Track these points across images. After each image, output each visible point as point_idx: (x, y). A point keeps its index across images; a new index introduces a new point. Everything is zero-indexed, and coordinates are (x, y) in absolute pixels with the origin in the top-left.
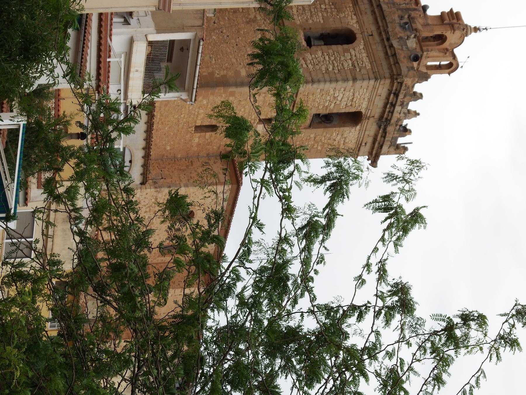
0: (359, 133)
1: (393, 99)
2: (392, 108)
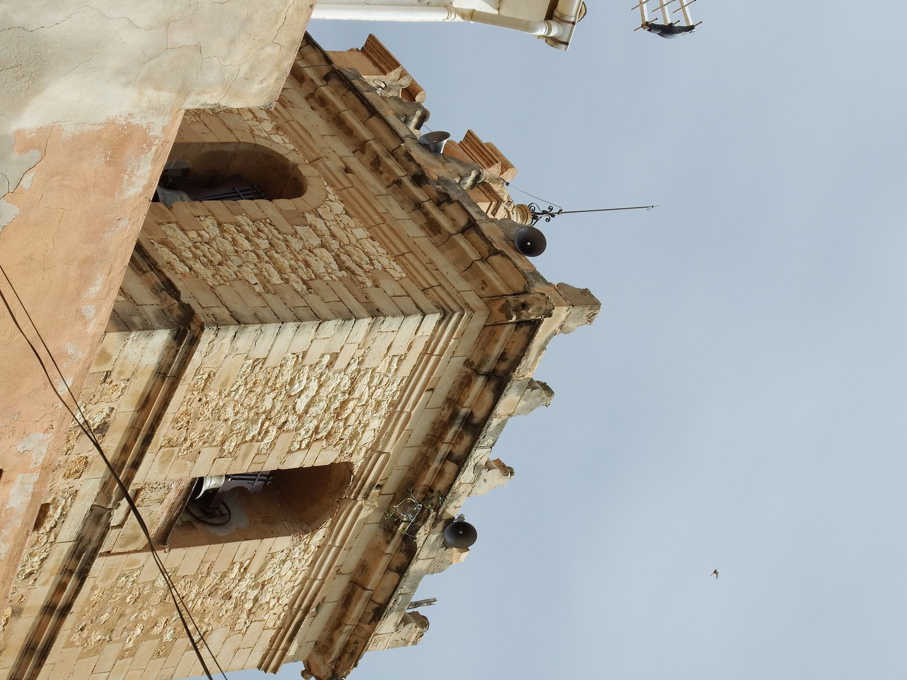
0: (314, 562)
1: (480, 397)
2: (467, 440)
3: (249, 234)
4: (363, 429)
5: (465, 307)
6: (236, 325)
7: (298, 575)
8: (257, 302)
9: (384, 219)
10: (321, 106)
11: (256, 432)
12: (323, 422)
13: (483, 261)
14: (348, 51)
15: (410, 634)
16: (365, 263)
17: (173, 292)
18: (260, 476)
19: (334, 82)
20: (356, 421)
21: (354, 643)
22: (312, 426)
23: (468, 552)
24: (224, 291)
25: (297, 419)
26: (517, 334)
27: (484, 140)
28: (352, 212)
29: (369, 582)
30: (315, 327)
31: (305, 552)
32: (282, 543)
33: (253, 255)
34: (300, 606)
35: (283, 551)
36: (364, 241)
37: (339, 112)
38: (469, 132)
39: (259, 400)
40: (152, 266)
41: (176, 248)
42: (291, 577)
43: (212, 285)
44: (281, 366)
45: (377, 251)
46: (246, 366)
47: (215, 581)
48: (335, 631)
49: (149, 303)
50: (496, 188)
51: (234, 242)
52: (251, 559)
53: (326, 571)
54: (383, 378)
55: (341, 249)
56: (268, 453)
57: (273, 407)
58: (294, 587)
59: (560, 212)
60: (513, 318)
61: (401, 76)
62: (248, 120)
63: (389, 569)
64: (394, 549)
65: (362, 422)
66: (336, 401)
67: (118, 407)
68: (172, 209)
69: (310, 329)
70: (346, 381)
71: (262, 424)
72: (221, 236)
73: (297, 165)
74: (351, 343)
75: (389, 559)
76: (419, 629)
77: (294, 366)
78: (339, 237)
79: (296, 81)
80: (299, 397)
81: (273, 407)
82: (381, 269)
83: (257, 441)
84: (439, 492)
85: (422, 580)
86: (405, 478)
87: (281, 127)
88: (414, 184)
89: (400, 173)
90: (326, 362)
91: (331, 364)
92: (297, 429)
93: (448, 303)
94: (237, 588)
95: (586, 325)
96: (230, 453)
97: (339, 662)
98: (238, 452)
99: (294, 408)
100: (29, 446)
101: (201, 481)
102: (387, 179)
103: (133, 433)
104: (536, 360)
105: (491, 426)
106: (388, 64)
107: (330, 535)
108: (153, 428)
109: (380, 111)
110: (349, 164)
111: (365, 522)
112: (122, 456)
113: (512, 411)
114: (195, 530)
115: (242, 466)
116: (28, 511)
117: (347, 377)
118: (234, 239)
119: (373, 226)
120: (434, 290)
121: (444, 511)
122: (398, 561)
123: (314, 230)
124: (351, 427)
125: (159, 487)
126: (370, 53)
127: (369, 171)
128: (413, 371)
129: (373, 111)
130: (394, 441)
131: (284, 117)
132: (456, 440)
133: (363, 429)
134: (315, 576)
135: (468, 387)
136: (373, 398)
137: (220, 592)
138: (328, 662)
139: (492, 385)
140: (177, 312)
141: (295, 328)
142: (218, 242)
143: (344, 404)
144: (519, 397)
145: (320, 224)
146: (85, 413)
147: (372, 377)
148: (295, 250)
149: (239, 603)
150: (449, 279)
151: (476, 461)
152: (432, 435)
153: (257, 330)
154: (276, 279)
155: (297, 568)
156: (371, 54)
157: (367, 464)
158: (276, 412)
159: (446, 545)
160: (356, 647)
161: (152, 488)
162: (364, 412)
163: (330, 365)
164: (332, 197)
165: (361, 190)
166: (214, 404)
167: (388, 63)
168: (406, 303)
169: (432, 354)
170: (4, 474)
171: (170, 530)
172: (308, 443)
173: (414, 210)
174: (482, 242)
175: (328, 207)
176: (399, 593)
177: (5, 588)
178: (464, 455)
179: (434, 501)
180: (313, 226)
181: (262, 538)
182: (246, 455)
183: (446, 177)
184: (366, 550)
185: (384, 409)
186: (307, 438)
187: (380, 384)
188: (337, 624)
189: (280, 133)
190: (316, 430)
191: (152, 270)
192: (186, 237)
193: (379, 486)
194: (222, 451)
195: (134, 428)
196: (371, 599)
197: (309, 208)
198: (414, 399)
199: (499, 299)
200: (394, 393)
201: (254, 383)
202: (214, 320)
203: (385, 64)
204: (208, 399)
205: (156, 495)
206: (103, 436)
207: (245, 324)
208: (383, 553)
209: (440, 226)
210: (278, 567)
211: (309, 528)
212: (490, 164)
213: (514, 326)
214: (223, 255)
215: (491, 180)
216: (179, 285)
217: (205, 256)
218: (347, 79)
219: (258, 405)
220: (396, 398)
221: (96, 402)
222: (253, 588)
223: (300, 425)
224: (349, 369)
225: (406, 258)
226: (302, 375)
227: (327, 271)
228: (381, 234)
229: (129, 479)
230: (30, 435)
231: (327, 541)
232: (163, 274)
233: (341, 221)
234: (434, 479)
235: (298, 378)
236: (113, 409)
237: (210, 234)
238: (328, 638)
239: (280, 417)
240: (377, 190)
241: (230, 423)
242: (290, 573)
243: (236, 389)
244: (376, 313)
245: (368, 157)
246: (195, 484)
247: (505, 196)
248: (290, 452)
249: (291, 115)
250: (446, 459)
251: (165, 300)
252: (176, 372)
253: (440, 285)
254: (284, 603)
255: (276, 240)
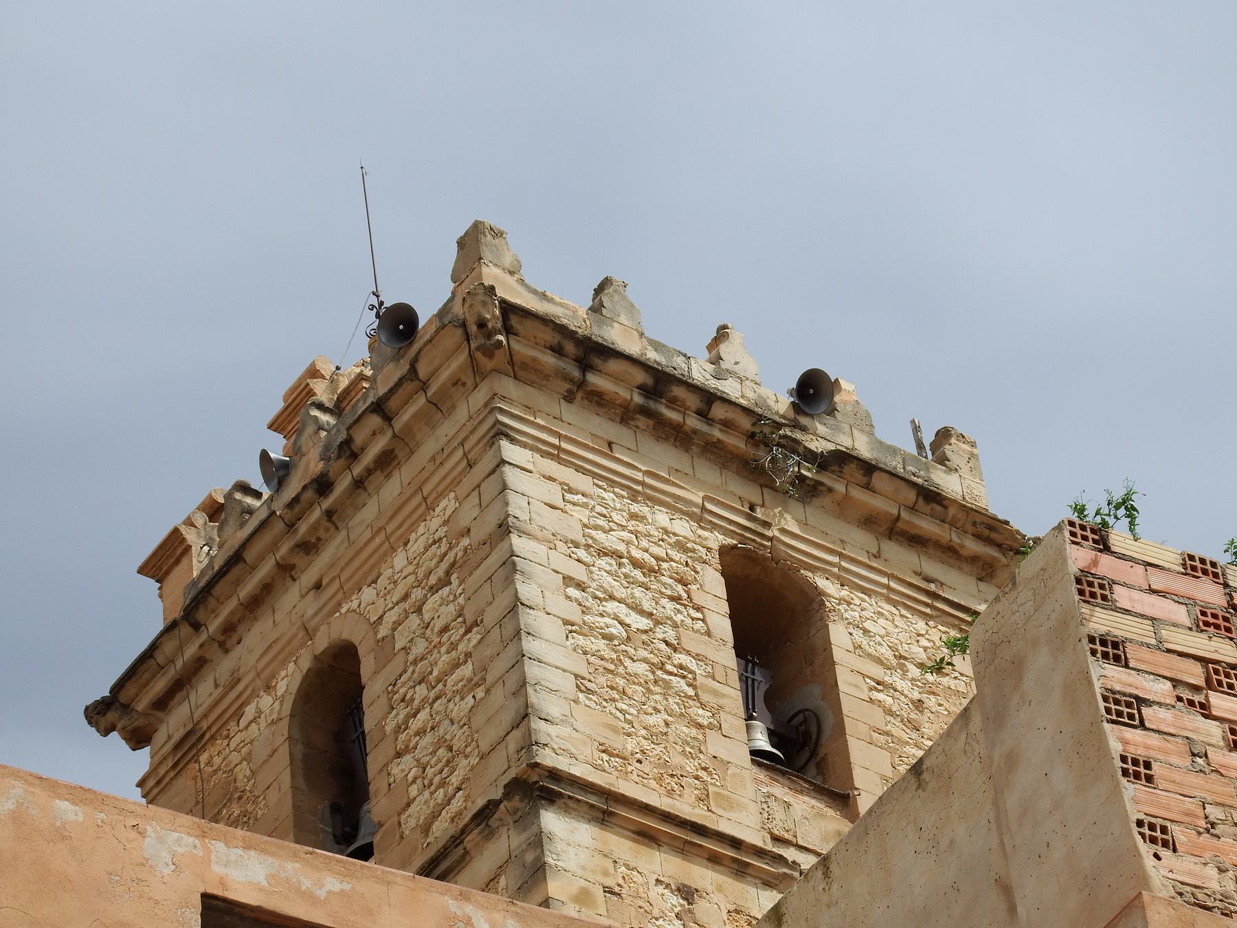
1: (616, 379)
2: (678, 391)
3: (408, 713)
4: (671, 535)
5: (489, 408)
6: (529, 721)
7: (883, 611)
8: (498, 693)
9: (381, 529)
10: (235, 631)
11: (682, 682)
12: (664, 590)
13: (427, 388)
14: (162, 601)
15: (960, 452)
16: (439, 550)
17: (490, 810)
18: (747, 672)
19: (201, 615)
20: (660, 546)
21: (975, 526)
22: (670, 605)
23: (840, 380)
24: (487, 739)
25: (660, 626)
26: (522, 333)
27: (280, 405)
28: (374, 573)
29: (888, 513)
30: (528, 610)
31: (851, 603)
32: (839, 635)
33: (436, 705)
34: (927, 605)
35: (851, 634)
36: (410, 554)
37: (242, 604)
38: (270, 427)
39: (636, 680)
40: (456, 843)
41: (432, 812)
42: (887, 619)
43: (478, 758)
44: (585, 653)
45: (422, 535)
46: (587, 702)
47: (897, 724)
48: (961, 555)
49: (506, 842)
50: (344, 383)
51: (420, 733)
52: (864, 676)
53: (876, 573)
54: (596, 513)
55: (422, 585)
56: (711, 663)
57: (645, 660)
58: (900, 615)
59: (376, 295)
60: (500, 339)
61: (192, 525)
62: (259, 730)
63: (867, 487)
64: (838, 481)
65: (660, 537)
66: (633, 574)
67: (655, 873)
68: (382, 822)
69: (531, 617)
70: (603, 563)
71: (671, 674)
72: (414, 752)
73: (315, 656)
74: (548, 559)
75: (853, 487)
76: (953, 441)
77: (585, 635)
78: (406, 589)
79: (205, 668)
80: (629, 626)
81: (645, 660)
82: (446, 527)
83: (695, 679)
84: (754, 425)
85: (884, 441)
86: (738, 473)
87: (267, 683)
88: (330, 492)
89: (316, 514)
90: (577, 592)
91: (580, 585)
92: (675, 626)
93: (485, 431)
94: (906, 692)
95: (507, 239)
96: (713, 715)
97: (1004, 546)
98: (711, 704)
99: (646, 632)
100: (165, 856)
101: (756, 753)
102: (327, 530)
103: (690, 850)
104: (561, 305)
105: (658, 359)
106: (176, 544)
107: (824, 571)
108: (682, 823)
109: (237, 546)
110: (310, 585)
111: (804, 524)
112: (724, 863)
113: (635, 333)
114: (828, 756)
115: (732, 698)
116: (272, 854)
117: (597, 562)
118: (417, 734)
119: (390, 543)
120: (470, 451)
121: (783, 417)
122: (856, 474)
123: (400, 624)
124: (669, 551)
125: (767, 809)
126: (163, 571)
127: (318, 556)
128: (584, 472)
129: (236, 558)
130: (687, 492)
131: (253, 680)
132: (679, 406)
133: (671, 535)
134: (884, 587)
135: (603, 395)
136: (626, 525)
137: (913, 716)
138: (1005, 561)
139: (597, 361)
140: (516, 802)
141: (530, 638)
142: (422, 755)
143: (636, 564)
144: (615, 324)
145: (391, 617)
146: (666, 918)
147: (596, 527)
148: (427, 648)
149: (928, 689)
150: (454, 433)
151: (708, 377)
152: (675, 440)
153: (536, 691)
154: (466, 670)
155: (875, 613)
156: (165, 568)
157: (721, 527)
158: (652, 656)
159: (832, 411)
160: (981, 524)
161: (768, 819)
162: (646, 535)
163: (581, 586)
164: (354, 605)
165: (343, 565)
166: (644, 742)
167: (174, 544)
168: (489, 489)
169: (559, 448)
170: (211, 891)
171: (827, 790)
172: (694, 609)
173: (365, 490)
174: (401, 391)
175: (368, 608)
176: (902, 471)
177: (399, 880)
178: (699, 394)
179: (767, 430)
180: (394, 627)
181: (834, 663)
182: (716, 693)
183: (320, 449)
184: (843, 520)
185: (641, 509)
186: (687, 611)
187: (605, 516)
188: (950, 553)
189: (273, 684)
190: (676, 599)
191: (462, 841)
192: (418, 799)
193: (752, 508)
194: (711, 727)
195: (683, 850)
196: (912, 508)
197: (371, 633)
198: (625, 469)
199: (476, 360)
200: (617, 497)
201: (612, 690)
202: (524, 751)
203: (175, 549)
204: (638, 751)
205: (779, 813)
206: (697, 891)
207: (527, 707)
208: (847, 496)
209: (383, 452)
210: (874, 639)
211: (817, 600)
212: (311, 393)
213: (512, 337)
214: (438, 746)
215: (334, 391)
216: (480, 803)
217: (441, 772)
218: (195, 598)
219: (643, 682)
220: (624, 493)
221: (648, 904)
222: (905, 671)
223: (668, 621)
224: (585, 560)
225: (429, 494)
226: (597, 624)
227: (453, 601)
228: (399, 532)
229: (756, 851)
230: (147, 857)
231: (833, 575)
232: (466, 826)
233: (385, 588)
234: (736, 433)
235: (602, 628)
236: (657, 880)
237: (411, 767)
238: (971, 564)
239: (658, 650)
240: (342, 543)
241: (670, 719)
242: (881, 621)
243: (621, 713)
244: (504, 529)
245: (300, 560)
246: (761, 760)
247: (355, 371)
248: (708, 633)
249: (250, 671)
250: (706, 418)
251: (501, 820)
252: (600, 796)
253: (462, 444)
254: (925, 626)
255: (415, 675)
